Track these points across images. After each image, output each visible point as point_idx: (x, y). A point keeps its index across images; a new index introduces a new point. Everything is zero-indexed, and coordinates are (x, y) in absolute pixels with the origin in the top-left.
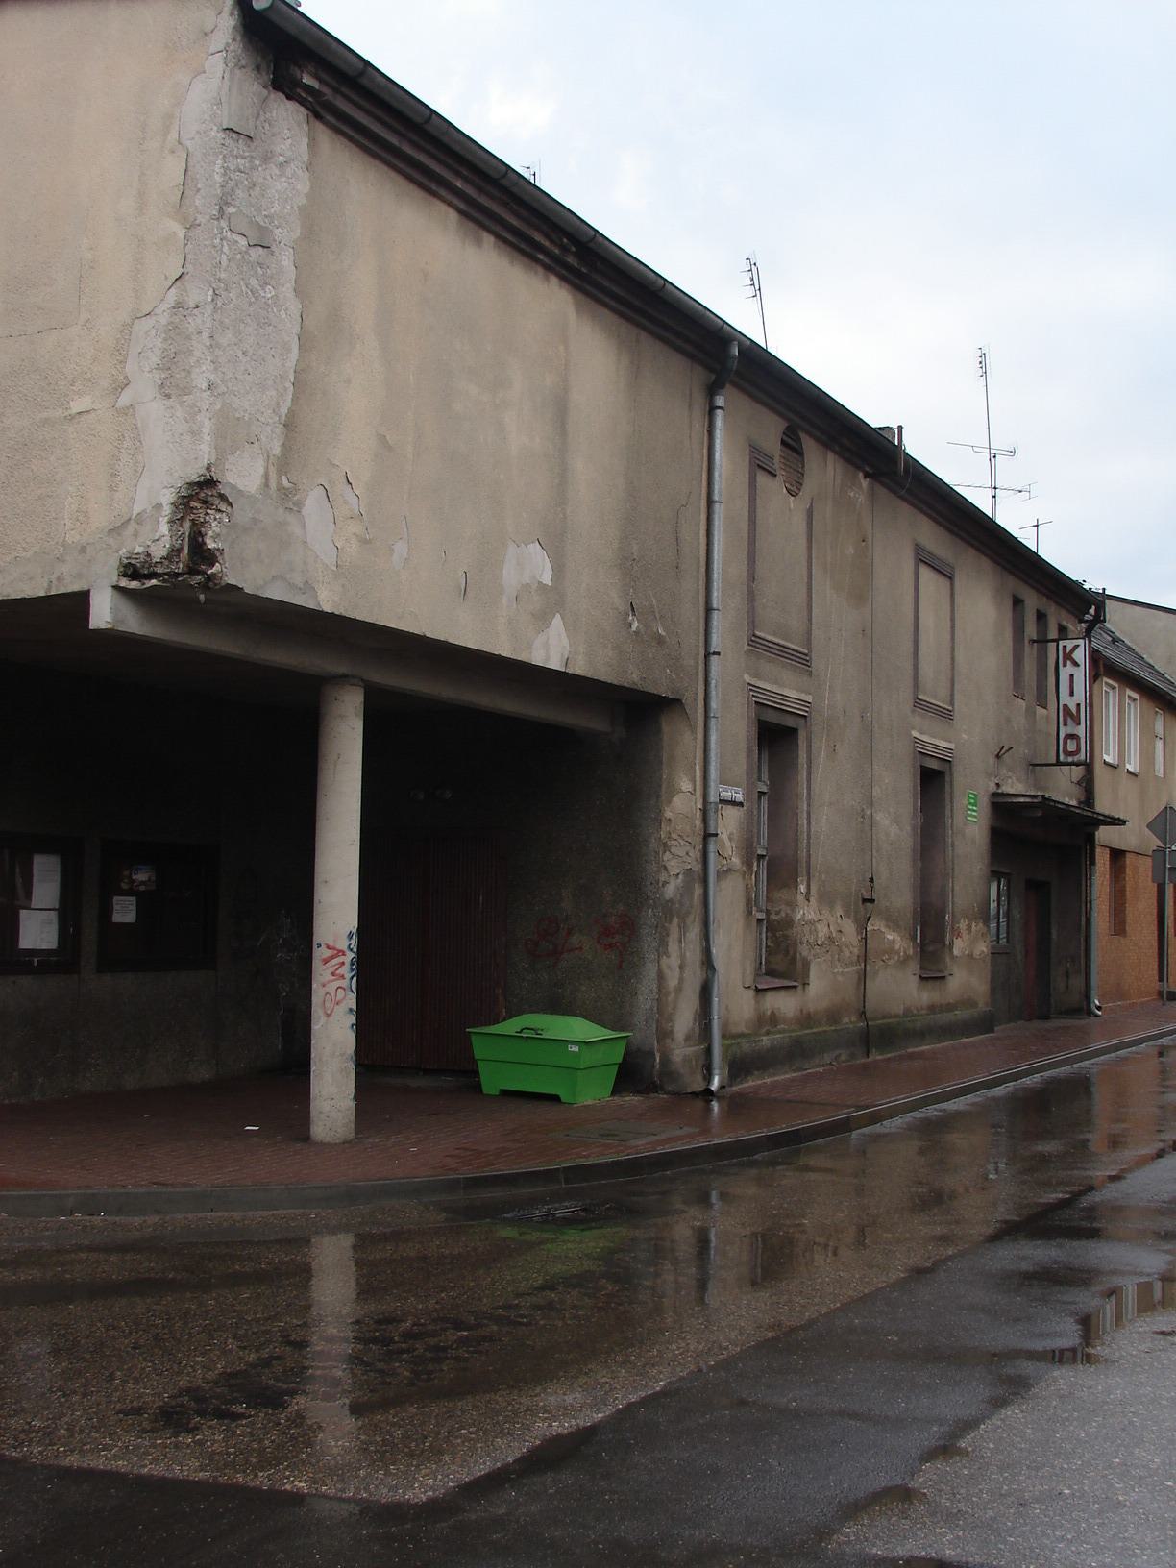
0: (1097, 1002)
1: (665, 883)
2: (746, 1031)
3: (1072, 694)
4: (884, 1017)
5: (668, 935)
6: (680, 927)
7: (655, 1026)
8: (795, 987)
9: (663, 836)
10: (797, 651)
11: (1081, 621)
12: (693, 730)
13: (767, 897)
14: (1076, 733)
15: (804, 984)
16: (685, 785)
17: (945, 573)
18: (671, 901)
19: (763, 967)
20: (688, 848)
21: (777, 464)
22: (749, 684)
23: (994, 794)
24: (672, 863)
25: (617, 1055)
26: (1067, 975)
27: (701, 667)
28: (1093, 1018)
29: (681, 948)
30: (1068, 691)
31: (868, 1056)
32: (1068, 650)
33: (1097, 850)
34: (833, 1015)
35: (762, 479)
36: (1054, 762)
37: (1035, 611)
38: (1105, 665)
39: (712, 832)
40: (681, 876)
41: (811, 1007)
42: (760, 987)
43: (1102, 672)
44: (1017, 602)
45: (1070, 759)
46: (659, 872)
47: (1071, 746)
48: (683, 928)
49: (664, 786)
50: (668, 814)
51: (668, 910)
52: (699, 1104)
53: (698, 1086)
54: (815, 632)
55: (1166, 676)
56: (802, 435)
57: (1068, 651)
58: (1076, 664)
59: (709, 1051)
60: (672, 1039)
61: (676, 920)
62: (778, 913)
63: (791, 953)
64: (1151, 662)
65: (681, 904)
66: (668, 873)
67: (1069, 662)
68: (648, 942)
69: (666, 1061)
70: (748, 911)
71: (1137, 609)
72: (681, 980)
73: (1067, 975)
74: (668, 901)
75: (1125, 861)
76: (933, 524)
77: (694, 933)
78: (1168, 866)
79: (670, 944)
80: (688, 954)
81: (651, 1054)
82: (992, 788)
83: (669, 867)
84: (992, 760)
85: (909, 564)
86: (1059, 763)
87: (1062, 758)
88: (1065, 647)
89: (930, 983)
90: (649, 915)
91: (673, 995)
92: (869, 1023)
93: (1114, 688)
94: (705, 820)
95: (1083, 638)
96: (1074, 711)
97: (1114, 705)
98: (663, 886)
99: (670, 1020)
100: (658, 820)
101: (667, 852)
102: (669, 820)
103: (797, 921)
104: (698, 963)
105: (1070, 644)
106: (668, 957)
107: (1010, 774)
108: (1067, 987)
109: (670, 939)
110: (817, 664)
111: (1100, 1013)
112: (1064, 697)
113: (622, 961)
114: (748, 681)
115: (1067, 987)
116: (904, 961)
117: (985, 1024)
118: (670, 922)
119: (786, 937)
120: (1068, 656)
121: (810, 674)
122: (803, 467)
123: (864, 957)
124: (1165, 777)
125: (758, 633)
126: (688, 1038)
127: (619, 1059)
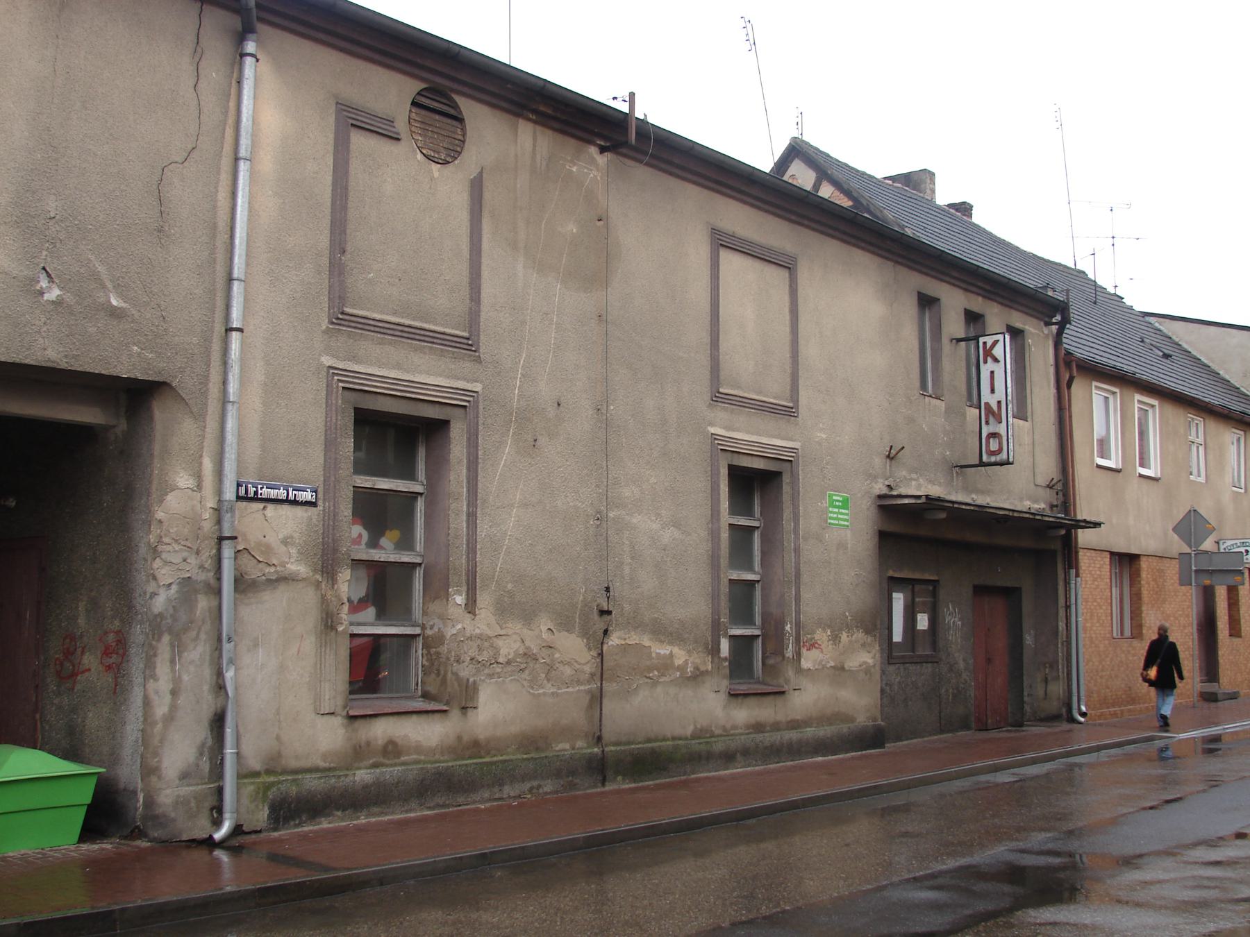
0: (1083, 709)
1: (154, 595)
2: (322, 764)
3: (993, 391)
4: (649, 740)
5: (155, 655)
6: (172, 646)
7: (139, 761)
8: (445, 711)
9: (152, 540)
10: (457, 336)
11: (1048, 324)
12: (200, 417)
13: (423, 610)
14: (997, 431)
15: (464, 709)
16: (184, 480)
17: (787, 264)
18: (160, 615)
19: (420, 688)
20: (185, 554)
21: (401, 126)
22: (330, 367)
23: (880, 497)
24: (163, 571)
25: (85, 793)
26: (1046, 681)
27: (216, 347)
28: (1075, 725)
29: (173, 671)
30: (989, 390)
31: (603, 785)
32: (988, 346)
33: (1080, 554)
34: (532, 742)
35: (359, 141)
36: (977, 463)
37: (963, 310)
38: (1078, 366)
39: (227, 534)
40: (174, 587)
41: (482, 735)
42: (352, 713)
43: (1075, 375)
44: (927, 302)
45: (993, 459)
46: (148, 581)
47: (994, 446)
48: (178, 648)
49: (155, 483)
50: (160, 515)
51: (157, 626)
52: (200, 855)
53: (200, 828)
54: (486, 312)
55: (1242, 389)
56: (461, 101)
57: (988, 348)
58: (996, 360)
59: (220, 791)
60: (159, 777)
61: (166, 639)
62: (432, 627)
63: (442, 672)
64: (1227, 377)
65: (175, 619)
66: (158, 583)
67: (989, 359)
68: (136, 664)
69: (150, 803)
70: (326, 626)
71: (1213, 329)
72: (173, 708)
73: (1046, 681)
74: (156, 616)
75: (1140, 564)
76: (787, 223)
77: (198, 652)
78: (1194, 568)
79: (158, 665)
80: (185, 678)
81: (135, 793)
82: (879, 488)
83: (159, 576)
84: (878, 462)
85: (698, 250)
86: (982, 464)
87: (985, 458)
88: (985, 343)
89: (740, 699)
90: (138, 634)
91: (159, 726)
92: (606, 749)
93: (1114, 393)
94: (219, 522)
95: (1003, 333)
96: (995, 408)
97: (1115, 410)
98: (151, 598)
99: (156, 754)
100: (148, 523)
101: (158, 559)
102: (160, 521)
103: (448, 637)
104: (206, 688)
105: (989, 340)
106: (156, 680)
107: (914, 476)
108: (1046, 694)
109: (159, 660)
110: (486, 345)
111: (1082, 719)
112: (986, 397)
113: (116, 686)
114: (329, 364)
115: (1046, 694)
116: (697, 677)
117: (872, 738)
118: (159, 640)
119: (438, 654)
120: (988, 353)
121: (478, 360)
122: (464, 135)
123: (601, 674)
124: (1206, 481)
125: (347, 310)
126: (184, 776)
127: (88, 799)
